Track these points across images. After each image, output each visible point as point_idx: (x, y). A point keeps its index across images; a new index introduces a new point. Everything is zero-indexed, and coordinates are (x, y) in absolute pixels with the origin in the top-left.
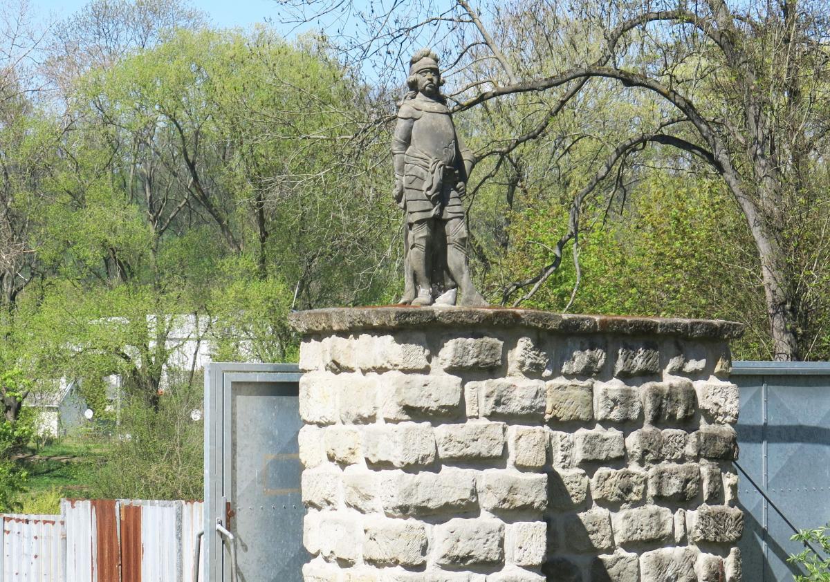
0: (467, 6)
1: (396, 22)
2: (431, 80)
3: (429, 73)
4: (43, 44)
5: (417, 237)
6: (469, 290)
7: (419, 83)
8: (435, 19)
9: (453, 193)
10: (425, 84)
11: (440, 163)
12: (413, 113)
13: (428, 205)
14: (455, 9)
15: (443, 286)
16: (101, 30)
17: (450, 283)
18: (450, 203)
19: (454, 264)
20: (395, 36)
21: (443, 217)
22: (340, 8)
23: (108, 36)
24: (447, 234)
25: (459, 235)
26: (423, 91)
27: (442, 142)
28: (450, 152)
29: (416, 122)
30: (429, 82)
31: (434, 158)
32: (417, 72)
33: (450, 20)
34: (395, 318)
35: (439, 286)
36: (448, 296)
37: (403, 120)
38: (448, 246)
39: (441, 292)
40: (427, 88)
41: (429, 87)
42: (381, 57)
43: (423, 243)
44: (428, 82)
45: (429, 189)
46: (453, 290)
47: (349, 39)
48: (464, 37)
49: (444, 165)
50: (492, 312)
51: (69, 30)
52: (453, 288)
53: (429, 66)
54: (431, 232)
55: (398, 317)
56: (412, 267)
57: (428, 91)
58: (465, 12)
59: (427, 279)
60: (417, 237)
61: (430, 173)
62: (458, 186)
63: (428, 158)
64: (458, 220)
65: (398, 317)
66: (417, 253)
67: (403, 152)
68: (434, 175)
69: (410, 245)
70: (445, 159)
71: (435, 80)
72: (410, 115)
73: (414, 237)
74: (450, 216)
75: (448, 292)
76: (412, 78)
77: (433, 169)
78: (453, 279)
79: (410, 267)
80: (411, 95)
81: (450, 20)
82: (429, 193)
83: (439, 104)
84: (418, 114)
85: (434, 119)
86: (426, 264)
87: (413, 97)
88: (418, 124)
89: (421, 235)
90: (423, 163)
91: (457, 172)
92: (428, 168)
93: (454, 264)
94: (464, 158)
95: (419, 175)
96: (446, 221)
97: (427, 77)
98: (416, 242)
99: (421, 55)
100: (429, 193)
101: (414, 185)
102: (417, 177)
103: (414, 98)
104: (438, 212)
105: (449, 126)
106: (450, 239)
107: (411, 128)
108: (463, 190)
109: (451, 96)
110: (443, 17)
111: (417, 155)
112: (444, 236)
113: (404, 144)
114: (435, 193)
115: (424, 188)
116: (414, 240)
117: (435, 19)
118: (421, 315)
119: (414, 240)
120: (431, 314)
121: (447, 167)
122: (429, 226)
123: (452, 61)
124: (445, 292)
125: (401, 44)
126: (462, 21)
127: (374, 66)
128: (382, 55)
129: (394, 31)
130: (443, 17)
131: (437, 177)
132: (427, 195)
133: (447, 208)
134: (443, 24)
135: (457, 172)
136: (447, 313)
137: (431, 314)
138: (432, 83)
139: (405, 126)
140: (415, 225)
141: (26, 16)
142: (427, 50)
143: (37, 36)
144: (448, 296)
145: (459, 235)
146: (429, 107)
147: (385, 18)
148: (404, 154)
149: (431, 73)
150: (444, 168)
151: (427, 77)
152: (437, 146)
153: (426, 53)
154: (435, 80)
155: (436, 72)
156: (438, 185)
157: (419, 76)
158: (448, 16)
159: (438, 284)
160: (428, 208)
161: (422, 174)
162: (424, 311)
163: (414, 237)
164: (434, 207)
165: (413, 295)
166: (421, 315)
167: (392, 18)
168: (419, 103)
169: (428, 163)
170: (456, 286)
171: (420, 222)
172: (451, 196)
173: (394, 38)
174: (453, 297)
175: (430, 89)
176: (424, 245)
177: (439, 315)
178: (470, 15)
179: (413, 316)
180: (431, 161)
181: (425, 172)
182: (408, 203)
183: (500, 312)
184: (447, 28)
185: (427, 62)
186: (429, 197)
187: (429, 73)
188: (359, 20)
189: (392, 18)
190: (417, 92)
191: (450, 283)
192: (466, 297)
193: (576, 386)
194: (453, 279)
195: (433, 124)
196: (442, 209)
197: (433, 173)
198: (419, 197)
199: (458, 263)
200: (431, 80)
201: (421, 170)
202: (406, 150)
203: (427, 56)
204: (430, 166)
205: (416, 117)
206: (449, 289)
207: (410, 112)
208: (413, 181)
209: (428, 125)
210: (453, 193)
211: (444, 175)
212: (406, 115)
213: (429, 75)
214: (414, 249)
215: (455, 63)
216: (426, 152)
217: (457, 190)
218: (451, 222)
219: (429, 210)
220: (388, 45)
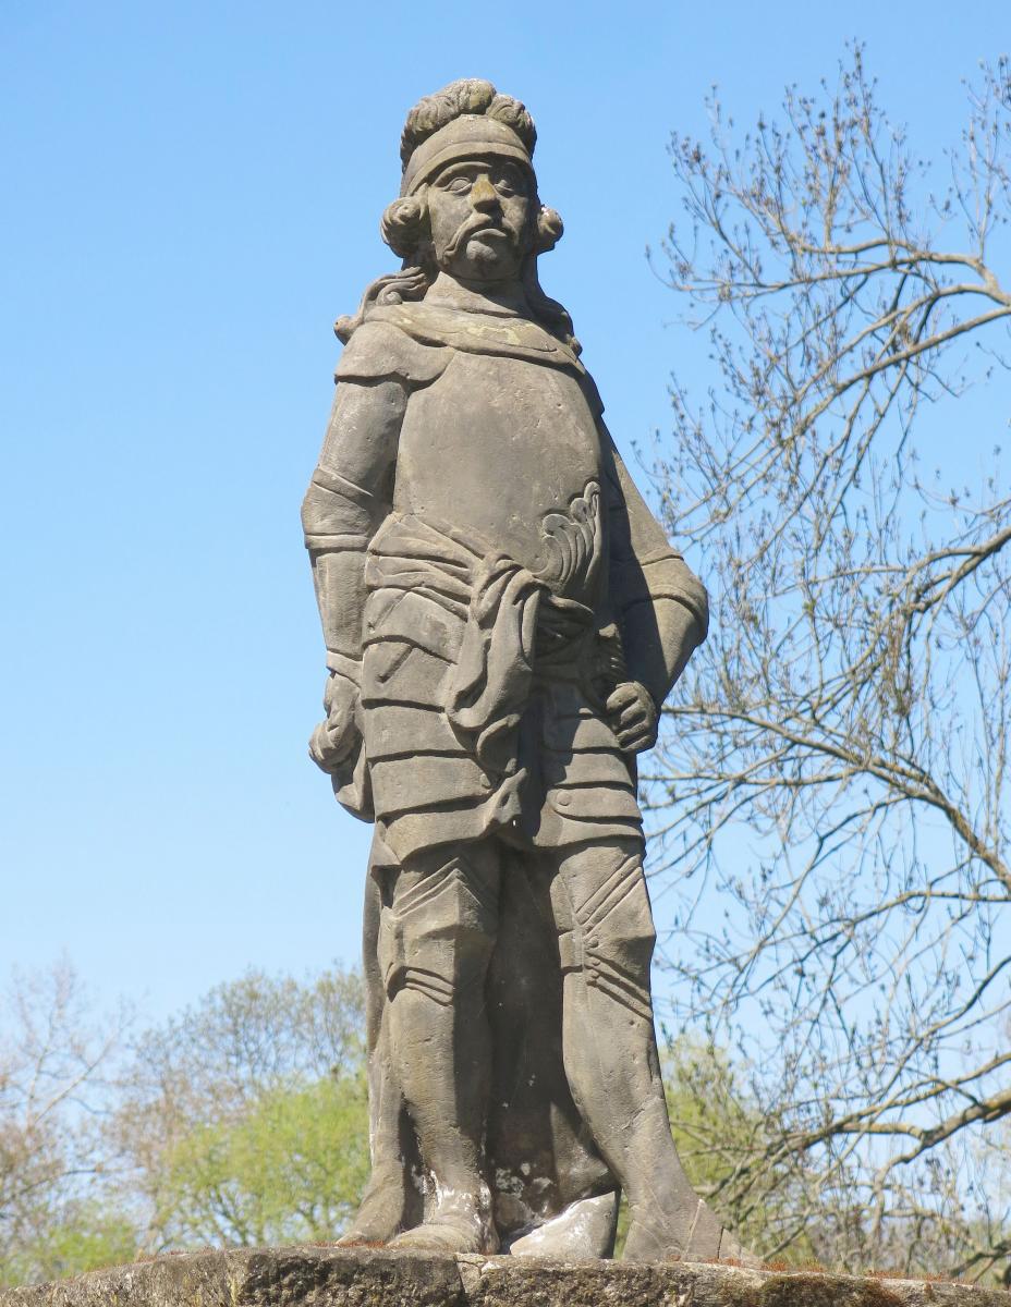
0: (998, 863)
1: (823, 902)
2: (491, 208)
3: (483, 179)
4: (110, 1071)
5: (413, 933)
6: (663, 1187)
7: (438, 226)
8: (920, 895)
9: (591, 731)
10: (461, 230)
11: (524, 576)
12: (400, 356)
13: (466, 777)
14: (966, 867)
15: (546, 1182)
16: (243, 1047)
17: (580, 1166)
18: (576, 770)
19: (594, 1064)
20: (820, 939)
21: (539, 840)
22: (683, 867)
23: (255, 1060)
24: (560, 920)
25: (617, 925)
26: (459, 266)
27: (536, 488)
28: (576, 533)
29: (417, 398)
30: (484, 217)
31: (492, 554)
32: (429, 180)
33: (956, 896)
34: (249, 1288)
35: (527, 1180)
36: (569, 1227)
37: (356, 388)
38: (568, 980)
39: (537, 1208)
40: (474, 247)
41: (486, 240)
42: (785, 994)
43: (443, 960)
44: (476, 218)
45: (467, 697)
46: (596, 1201)
47: (702, 940)
48: (989, 941)
49: (545, 591)
50: (758, 1283)
51: (171, 1044)
52: (598, 1189)
53: (481, 148)
54: (482, 913)
55: (265, 1283)
56: (393, 1082)
57: (480, 258)
58: (992, 875)
59: (467, 1141)
60: (413, 933)
61: (473, 624)
62: (613, 699)
63: (467, 555)
64: (611, 853)
65: (265, 1283)
66: (416, 1011)
67: (358, 539)
68: (494, 633)
69: (386, 976)
70: (550, 564)
71: (513, 212)
72: (387, 365)
73: (399, 935)
74: (571, 832)
75: (572, 1211)
76: (407, 206)
77: (486, 604)
78: (596, 1152)
79: (383, 1083)
80: (399, 284)
81: (956, 896)
82: (469, 717)
83: (531, 325)
84: (423, 361)
85: (499, 379)
86: (461, 1071)
87: (412, 294)
88: (425, 408)
89: (433, 924)
90: (439, 576)
91: (609, 630)
92: (466, 600)
93: (594, 1064)
94: (653, 590)
95: (424, 636)
96: (553, 858)
97: (471, 199)
98: (407, 963)
99: (450, 103)
100: (469, 717)
101: (397, 688)
102: (415, 645)
103: (419, 296)
104: (510, 810)
105: (573, 419)
106: (572, 946)
107: (395, 425)
108: (638, 717)
109: (959, 1082)
110: (937, 889)
111: (414, 544)
112: (549, 932)
113: (360, 500)
114: (493, 717)
115: (445, 696)
116: (401, 948)
117: (920, 895)
118: (385, 1277)
119: (401, 948)
120: (439, 1276)
121: (560, 601)
122: (471, 879)
123: (959, 1002)
124: (558, 1209)
125: (835, 957)
126: (985, 900)
127: (766, 1013)
128: (789, 986)
129: (816, 924)
130: (937, 889)
131: (509, 640)
132: (456, 727)
133: (556, 796)
134: (937, 907)
135: (609, 630)
136: (525, 1275)
137: (439, 1276)
138: (496, 222)
139: (363, 416)
140: (404, 876)
141: (69, 1011)
142: (479, 83)
143: (93, 1050)
144: (569, 1227)
145: (617, 925)
146: (479, 332)
147: (792, 890)
148: (363, 549)
149: (494, 180)
150: (544, 604)
151: (471, 199)
152: (511, 505)
153: (474, 100)
154: (513, 212)
155: (518, 176)
156: (513, 678)
157: (435, 197)
158: (950, 885)
159: (526, 1168)
160: (462, 789)
161: (438, 627)
162: (402, 1261)
163: (399, 935)
164: (495, 785)
165: (394, 1214)
166: (385, 1277)
167: (810, 894)
168: (438, 317)
169: (467, 580)
170: (611, 1183)
171: (427, 860)
172: (577, 743)
173: (819, 944)
174: (593, 1231)
175: (487, 249)
176: (449, 971)
177: (485, 1285)
178: (1004, 883)
179: (346, 1281)
180: (480, 570)
181: (451, 622)
182: (376, 770)
183: (803, 1282)
184: (948, 917)
185: (488, 134)
186: (467, 735)
187: (483, 179)
188: (729, 900)
189: (810, 894)
190: (430, 272)
191: (580, 1166)
192: (651, 1222)
193: (454, 540)
194: (596, 1152)
195: (496, 403)
196: (532, 798)
197: (487, 621)
198: (423, 741)
199: (610, 1058)
200: (491, 208)
201: (434, 610)
202: (372, 529)
203: (480, 109)
204: (473, 591)
205: (416, 376)
206: (577, 1197)
207: (386, 348)
208: (397, 664)
209: (471, 408)
210: (591, 731)
211: (539, 632)
212: (370, 360)
213: (483, 189)
214: (401, 994)
215: (970, 1005)
216: (456, 530)
217: (610, 717)
218: (576, 862)
219: (470, 802)
220: (802, 961)
